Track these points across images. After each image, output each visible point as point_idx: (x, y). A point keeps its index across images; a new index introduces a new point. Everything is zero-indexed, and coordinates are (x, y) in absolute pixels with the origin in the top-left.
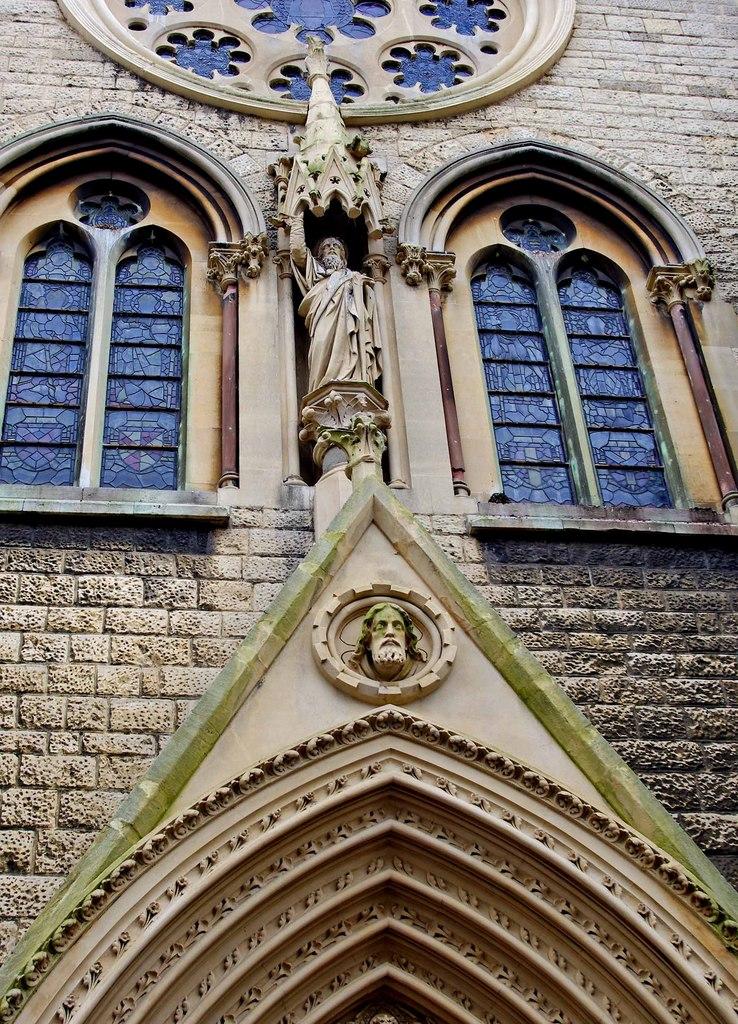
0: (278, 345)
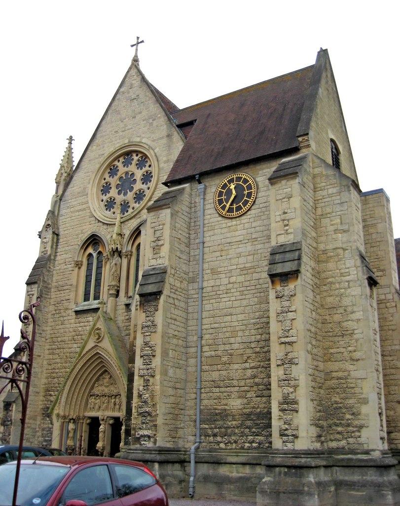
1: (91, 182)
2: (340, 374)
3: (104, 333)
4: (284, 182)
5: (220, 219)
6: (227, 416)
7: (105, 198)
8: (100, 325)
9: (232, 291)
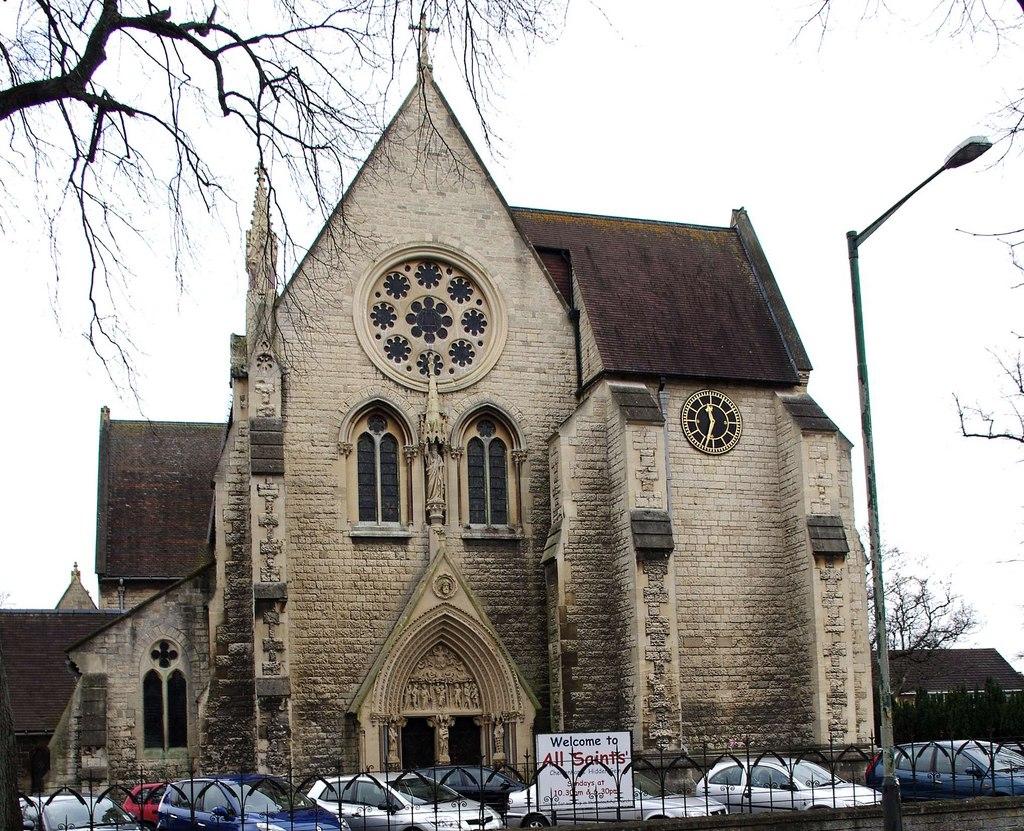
0: (421, 481)
4: (818, 437)
5: (691, 450)
6: (714, 710)
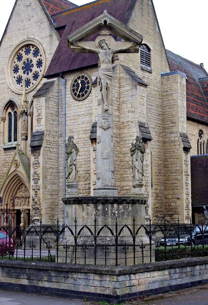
1: (7, 64)
2: (127, 188)
3: (19, 163)
5: (74, 100)
7: (16, 75)
8: (17, 158)
9: (80, 142)
